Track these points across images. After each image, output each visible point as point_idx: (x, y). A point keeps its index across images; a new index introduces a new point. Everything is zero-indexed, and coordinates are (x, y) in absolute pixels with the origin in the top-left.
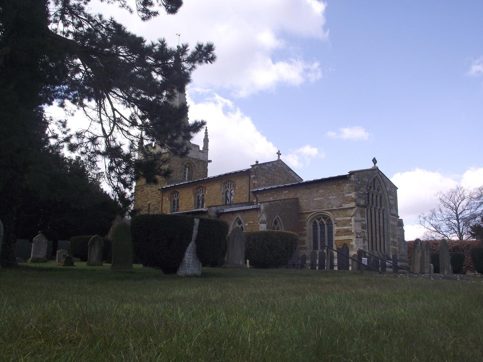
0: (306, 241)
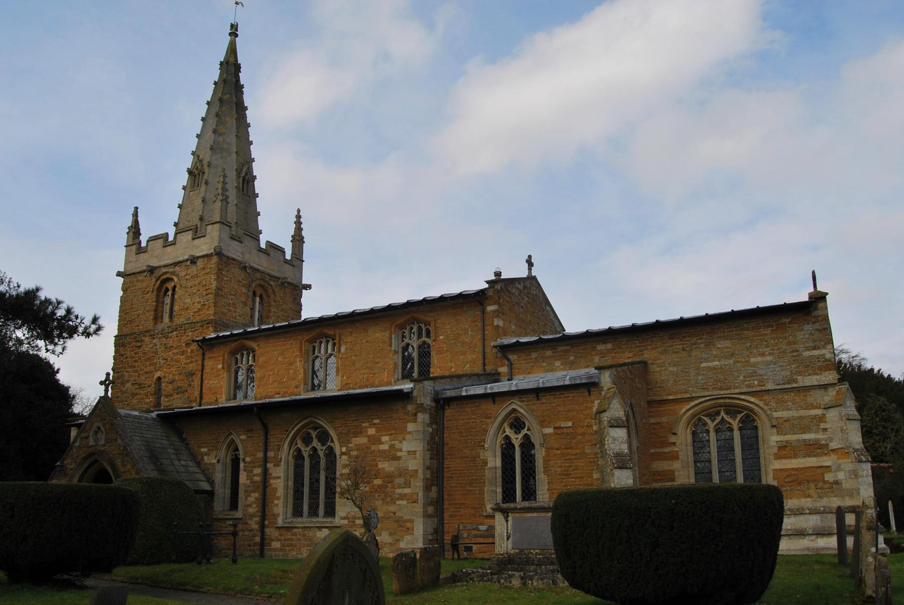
0: (676, 473)
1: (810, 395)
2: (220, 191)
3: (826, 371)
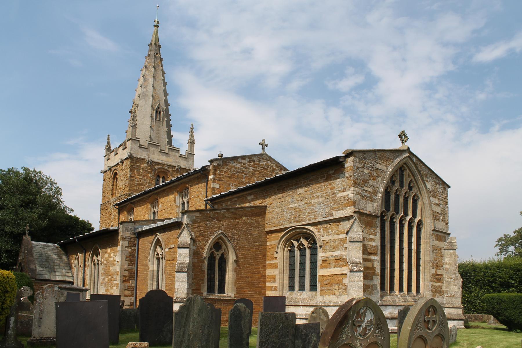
1: (341, 225)
3: (348, 207)
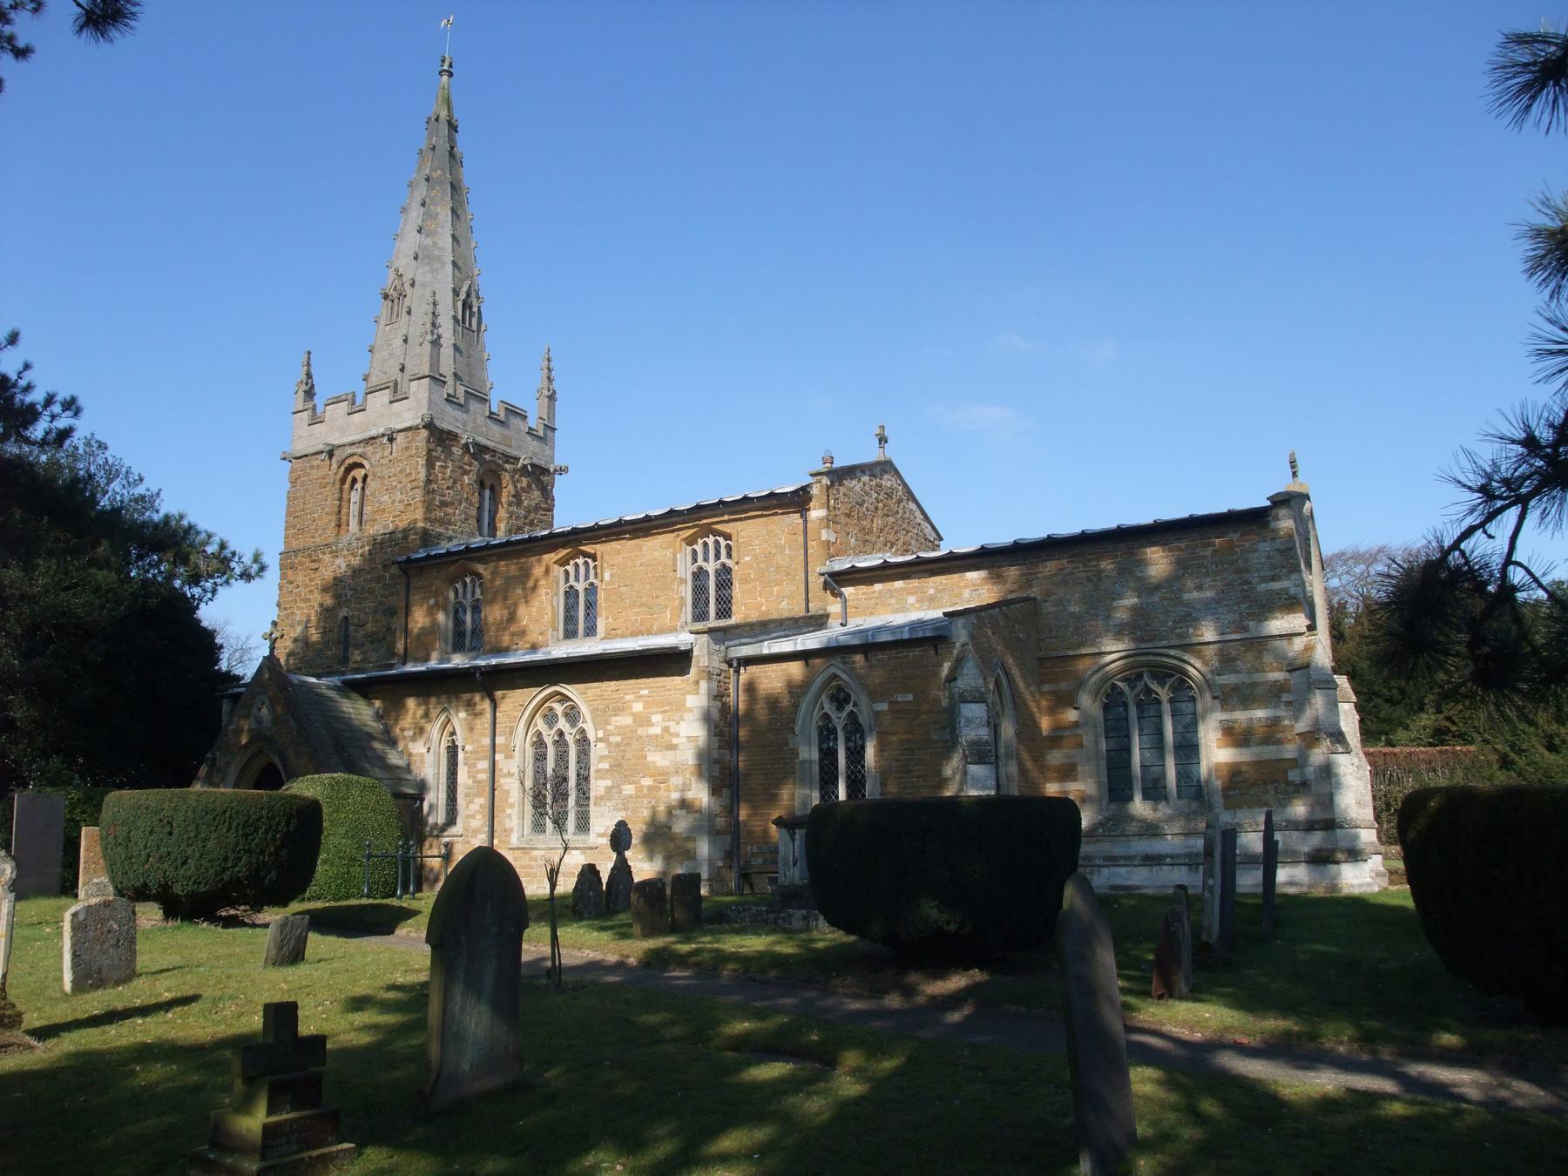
2: (429, 327)
